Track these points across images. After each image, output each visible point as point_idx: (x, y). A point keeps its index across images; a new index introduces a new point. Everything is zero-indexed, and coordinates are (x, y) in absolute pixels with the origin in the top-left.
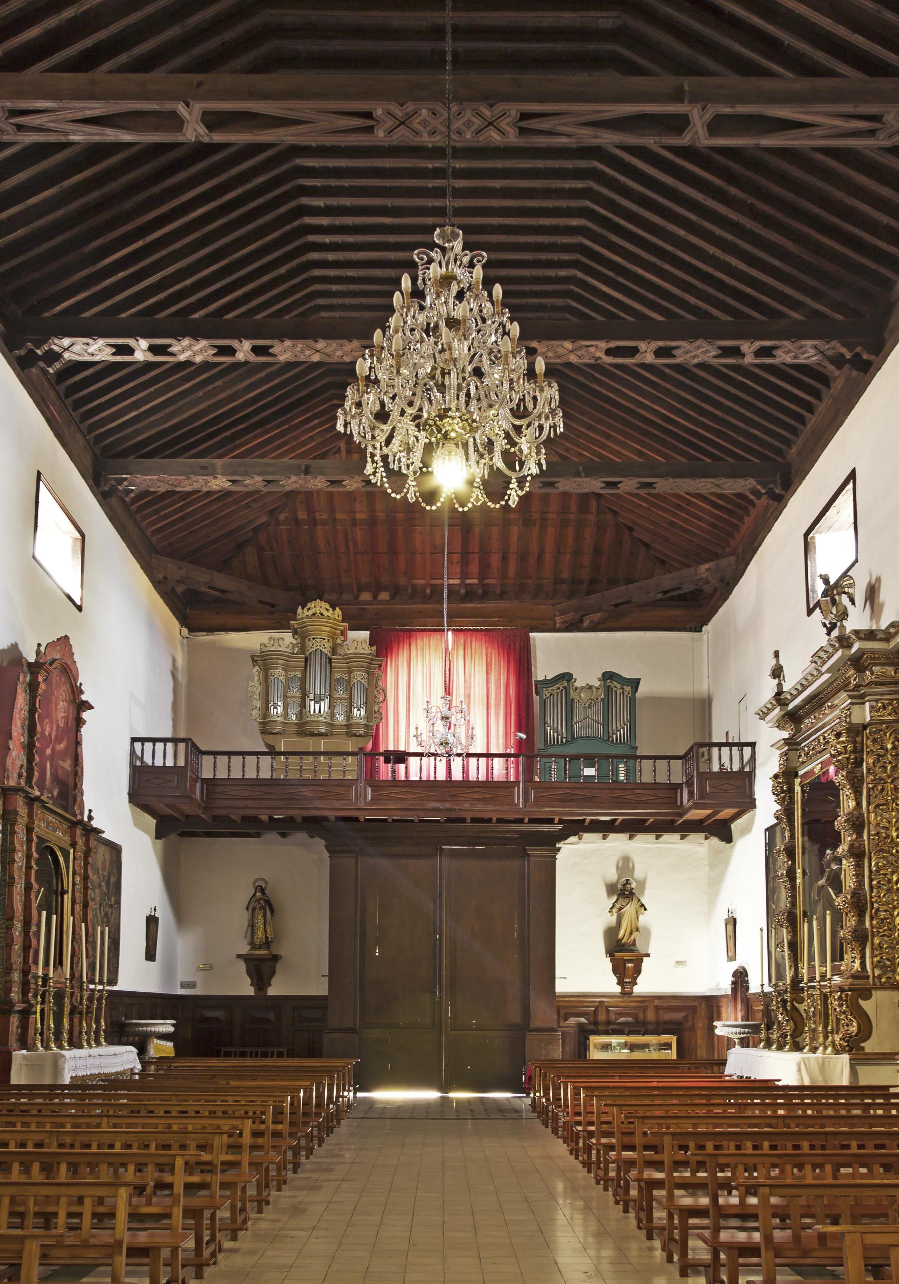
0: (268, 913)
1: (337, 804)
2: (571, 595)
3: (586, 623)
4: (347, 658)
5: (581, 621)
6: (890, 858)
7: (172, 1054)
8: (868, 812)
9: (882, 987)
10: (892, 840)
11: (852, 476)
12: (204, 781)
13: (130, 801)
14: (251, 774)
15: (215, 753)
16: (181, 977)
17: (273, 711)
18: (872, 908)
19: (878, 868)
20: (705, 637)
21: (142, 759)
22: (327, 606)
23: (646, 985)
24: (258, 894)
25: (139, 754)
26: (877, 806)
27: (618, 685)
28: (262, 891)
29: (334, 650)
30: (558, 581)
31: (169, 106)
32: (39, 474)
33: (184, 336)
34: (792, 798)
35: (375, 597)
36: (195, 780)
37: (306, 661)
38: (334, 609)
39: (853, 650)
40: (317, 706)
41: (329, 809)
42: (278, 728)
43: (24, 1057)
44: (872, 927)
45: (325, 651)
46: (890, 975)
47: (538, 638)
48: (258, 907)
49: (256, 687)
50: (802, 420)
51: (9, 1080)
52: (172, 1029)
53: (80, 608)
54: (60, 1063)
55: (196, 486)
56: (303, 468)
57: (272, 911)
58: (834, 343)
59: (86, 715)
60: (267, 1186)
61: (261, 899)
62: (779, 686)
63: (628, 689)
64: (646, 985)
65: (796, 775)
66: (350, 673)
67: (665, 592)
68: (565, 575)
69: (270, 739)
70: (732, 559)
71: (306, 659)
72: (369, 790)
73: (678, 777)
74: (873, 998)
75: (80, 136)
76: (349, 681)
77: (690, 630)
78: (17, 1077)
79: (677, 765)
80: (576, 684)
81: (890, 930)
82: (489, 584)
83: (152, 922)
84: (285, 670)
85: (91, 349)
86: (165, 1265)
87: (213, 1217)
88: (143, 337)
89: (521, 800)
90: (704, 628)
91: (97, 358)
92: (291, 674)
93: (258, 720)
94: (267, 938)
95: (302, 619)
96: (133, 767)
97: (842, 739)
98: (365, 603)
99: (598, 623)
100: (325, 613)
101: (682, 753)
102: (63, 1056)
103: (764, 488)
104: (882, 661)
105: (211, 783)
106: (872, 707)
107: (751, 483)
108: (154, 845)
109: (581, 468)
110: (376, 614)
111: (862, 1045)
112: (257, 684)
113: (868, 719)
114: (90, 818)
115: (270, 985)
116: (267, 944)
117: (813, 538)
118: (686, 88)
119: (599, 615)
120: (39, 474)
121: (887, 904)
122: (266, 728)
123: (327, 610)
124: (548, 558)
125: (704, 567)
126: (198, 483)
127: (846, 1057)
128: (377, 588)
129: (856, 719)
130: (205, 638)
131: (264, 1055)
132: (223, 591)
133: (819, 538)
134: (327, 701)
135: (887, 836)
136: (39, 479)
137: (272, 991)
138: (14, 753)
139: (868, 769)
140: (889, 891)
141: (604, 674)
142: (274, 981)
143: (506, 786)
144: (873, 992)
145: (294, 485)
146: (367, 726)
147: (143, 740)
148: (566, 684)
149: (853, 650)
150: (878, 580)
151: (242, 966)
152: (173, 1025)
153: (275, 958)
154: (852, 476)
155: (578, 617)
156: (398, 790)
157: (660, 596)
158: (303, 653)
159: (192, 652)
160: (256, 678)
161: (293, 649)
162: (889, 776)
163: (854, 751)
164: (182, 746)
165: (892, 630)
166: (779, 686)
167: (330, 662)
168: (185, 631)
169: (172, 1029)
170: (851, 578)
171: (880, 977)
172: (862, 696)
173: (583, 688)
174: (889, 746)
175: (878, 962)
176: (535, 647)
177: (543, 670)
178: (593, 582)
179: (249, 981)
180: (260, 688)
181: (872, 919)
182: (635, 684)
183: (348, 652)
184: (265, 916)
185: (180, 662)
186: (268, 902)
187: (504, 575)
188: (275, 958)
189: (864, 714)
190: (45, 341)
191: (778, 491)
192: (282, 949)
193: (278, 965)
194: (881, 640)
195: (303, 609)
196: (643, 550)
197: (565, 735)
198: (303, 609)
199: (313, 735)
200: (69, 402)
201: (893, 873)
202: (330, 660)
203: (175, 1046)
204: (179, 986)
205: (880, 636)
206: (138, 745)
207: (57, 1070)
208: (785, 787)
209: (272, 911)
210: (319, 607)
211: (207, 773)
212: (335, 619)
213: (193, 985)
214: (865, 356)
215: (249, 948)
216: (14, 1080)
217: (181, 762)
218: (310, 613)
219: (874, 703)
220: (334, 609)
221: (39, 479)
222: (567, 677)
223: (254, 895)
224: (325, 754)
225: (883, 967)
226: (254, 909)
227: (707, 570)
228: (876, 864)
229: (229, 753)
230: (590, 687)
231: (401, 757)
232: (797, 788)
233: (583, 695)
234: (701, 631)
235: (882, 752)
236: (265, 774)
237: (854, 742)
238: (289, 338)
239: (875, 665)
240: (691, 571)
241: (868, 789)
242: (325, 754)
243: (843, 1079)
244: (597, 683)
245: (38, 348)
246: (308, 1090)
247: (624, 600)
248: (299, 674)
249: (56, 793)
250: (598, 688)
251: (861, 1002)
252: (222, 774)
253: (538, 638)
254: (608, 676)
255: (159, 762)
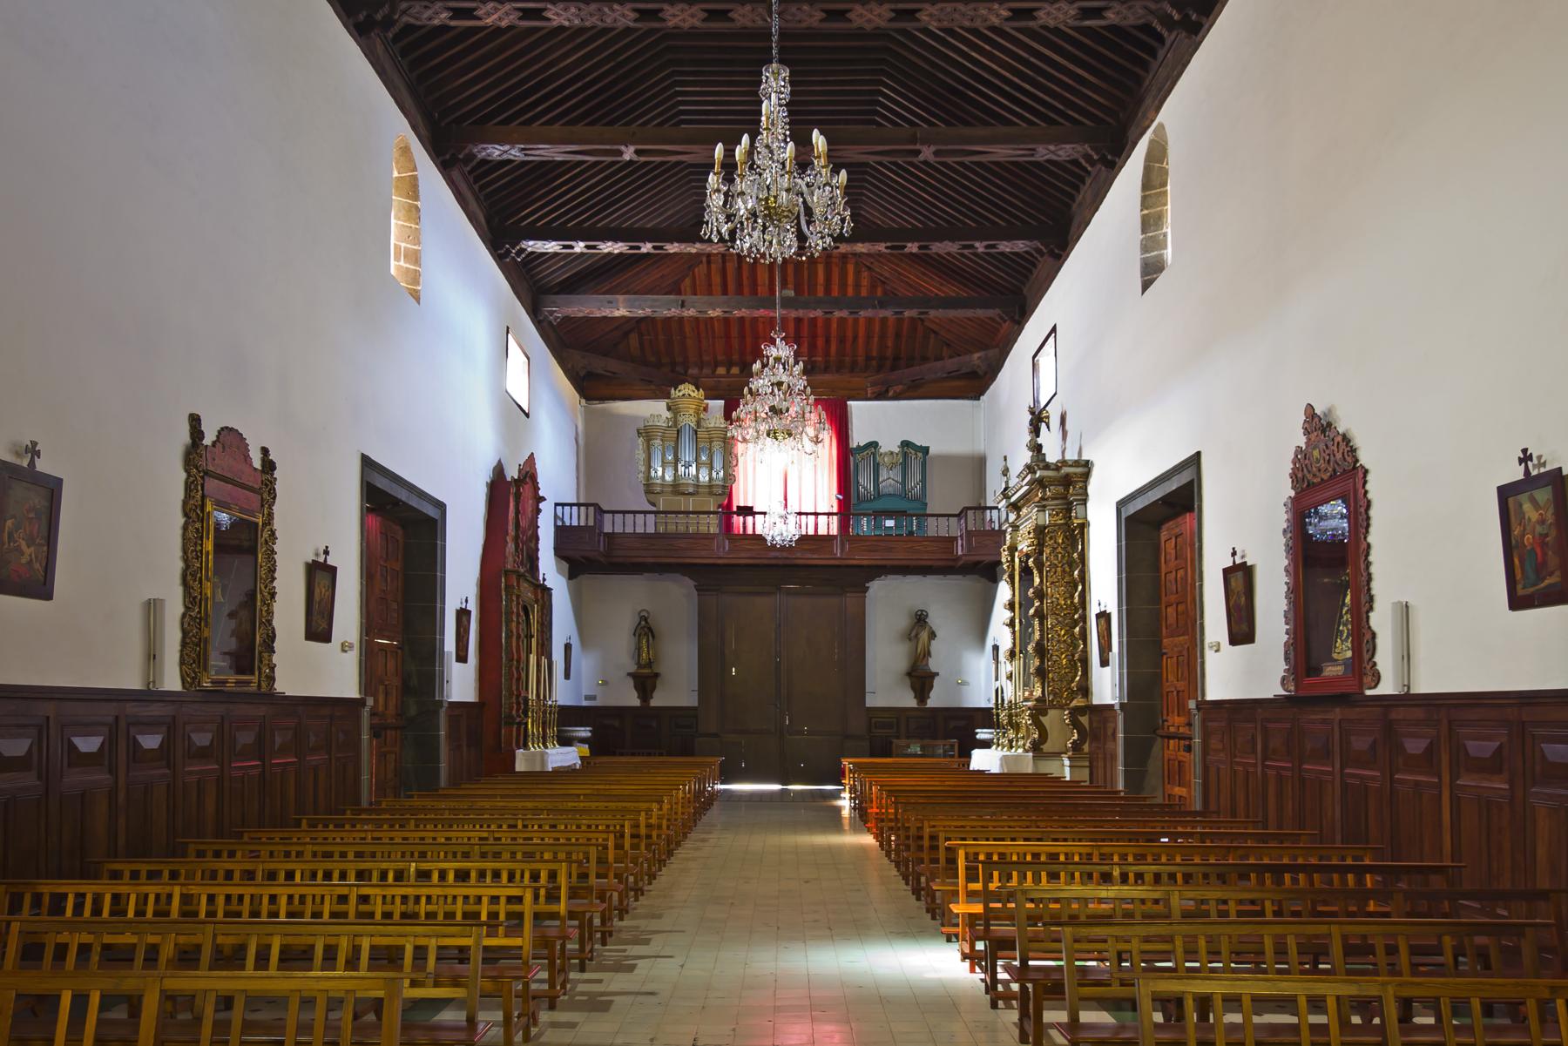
0: (651, 638)
1: (703, 553)
2: (879, 369)
3: (891, 394)
4: (708, 430)
5: (887, 391)
6: (1060, 619)
7: (588, 755)
8: (1047, 587)
9: (1054, 707)
10: (1062, 607)
11: (1054, 330)
12: (607, 534)
13: (555, 554)
14: (640, 530)
15: (614, 512)
16: (585, 692)
17: (653, 474)
18: (1048, 653)
19: (1052, 626)
20: (983, 405)
21: (562, 520)
22: (694, 388)
23: (933, 702)
24: (643, 623)
25: (561, 516)
26: (1052, 583)
27: (913, 452)
28: (646, 620)
29: (698, 424)
30: (868, 358)
31: (615, 147)
32: (508, 328)
33: (609, 241)
34: (1013, 566)
35: (728, 371)
36: (599, 535)
37: (678, 434)
38: (698, 391)
39: (1037, 476)
40: (687, 471)
41: (701, 557)
42: (658, 489)
43: (523, 754)
44: (1049, 666)
45: (692, 425)
46: (1059, 699)
47: (853, 405)
48: (643, 633)
49: (640, 455)
50: (1031, 272)
51: (514, 768)
52: (589, 734)
53: (527, 415)
54: (545, 758)
55: (604, 314)
56: (680, 302)
57: (653, 637)
58: (1035, 242)
59: (542, 505)
60: (591, 938)
61: (645, 627)
62: (1007, 482)
63: (920, 455)
64: (933, 702)
65: (1017, 550)
66: (711, 442)
67: (949, 373)
68: (874, 354)
69: (651, 497)
70: (997, 350)
71: (678, 431)
72: (727, 542)
73: (955, 532)
74: (1049, 715)
75: (559, 158)
76: (710, 449)
77: (971, 398)
78: (520, 766)
79: (953, 520)
80: (881, 450)
81: (1059, 668)
82: (815, 361)
83: (568, 647)
84: (662, 440)
85: (546, 247)
86: (516, 997)
87: (563, 946)
88: (582, 241)
89: (839, 551)
90: (981, 398)
91: (550, 251)
92: (667, 443)
93: (643, 482)
94: (650, 659)
95: (674, 398)
96: (556, 527)
97: (1031, 536)
98: (721, 376)
99: (900, 394)
100: (692, 394)
101: (958, 512)
102: (547, 753)
103: (1097, 154)
104: (1056, 483)
105: (611, 536)
106: (1049, 515)
107: (998, 311)
108: (568, 583)
109: (876, 302)
110: (729, 386)
111: (1042, 747)
112: (641, 452)
113: (1047, 522)
114: (544, 580)
115: (652, 698)
116: (650, 664)
117: (1038, 361)
118: (918, 135)
119: (901, 387)
120: (508, 328)
121: (1057, 651)
122: (649, 488)
123: (694, 391)
124: (861, 341)
125: (976, 355)
126: (607, 312)
127: (1031, 754)
128: (729, 365)
129: (1041, 522)
130: (599, 406)
131: (649, 754)
132: (614, 373)
133: (1041, 358)
134: (694, 466)
135: (1058, 604)
136: (508, 332)
137: (653, 703)
138: (509, 545)
139: (1047, 558)
140: (1059, 641)
141: (902, 442)
142: (655, 694)
143: (828, 538)
144: (1049, 711)
145: (673, 314)
146: (724, 487)
147: (563, 505)
148: (873, 450)
149: (1037, 476)
150: (1065, 413)
151: (631, 682)
152: (590, 731)
153: (657, 675)
154: (1054, 330)
155: (884, 389)
156: (747, 542)
157: (945, 375)
158: (676, 426)
159: (589, 418)
160: (641, 447)
161: (668, 423)
162: (1059, 563)
163: (1039, 544)
164: (591, 509)
165: (1059, 465)
166: (1007, 482)
167: (696, 434)
168: (583, 401)
169: (589, 734)
170: (1047, 412)
171: (1053, 700)
172: (1044, 506)
173: (886, 454)
174: (1060, 541)
175: (1052, 690)
176: (851, 414)
177: (858, 438)
178: (896, 358)
179: (636, 694)
180: (644, 456)
181: (1048, 661)
182: (926, 450)
183: (709, 426)
184: (648, 641)
185: (580, 428)
186: (650, 630)
187: (827, 353)
188: (657, 675)
189: (1046, 519)
190: (518, 244)
191: (1017, 318)
192: (660, 668)
193: (658, 682)
194: (1053, 470)
195: (675, 390)
196: (933, 336)
197: (872, 493)
198: (675, 390)
199: (684, 494)
200: (476, 187)
201: (1061, 629)
202: (696, 432)
203: (589, 748)
204: (583, 698)
205: (1053, 467)
206: (559, 508)
207: (543, 762)
208: (1009, 559)
209: (653, 637)
210: (687, 389)
211: (608, 529)
212: (699, 399)
213: (593, 698)
214: (1057, 251)
215: (636, 667)
216: (517, 769)
217: (591, 523)
218: (681, 394)
219: (1051, 512)
220: (698, 391)
221: (508, 332)
222: (874, 445)
223: (640, 623)
224: (693, 513)
225: (1055, 694)
226: (640, 635)
227: (979, 358)
228: (1051, 623)
229: (624, 512)
230: (892, 453)
231: (747, 511)
232: (1017, 560)
233: (886, 459)
234: (979, 399)
235: (1056, 546)
236: (651, 530)
237: (1039, 539)
238: (678, 242)
239: (1051, 485)
240: (967, 358)
241: (1047, 572)
242: (693, 513)
243: (1029, 768)
244: (897, 450)
245: (513, 249)
246: (648, 811)
247: (919, 377)
248: (673, 444)
249: (528, 566)
250: (897, 454)
251: (1041, 718)
252: (619, 529)
253: (853, 405)
254: (906, 444)
255: (575, 523)
